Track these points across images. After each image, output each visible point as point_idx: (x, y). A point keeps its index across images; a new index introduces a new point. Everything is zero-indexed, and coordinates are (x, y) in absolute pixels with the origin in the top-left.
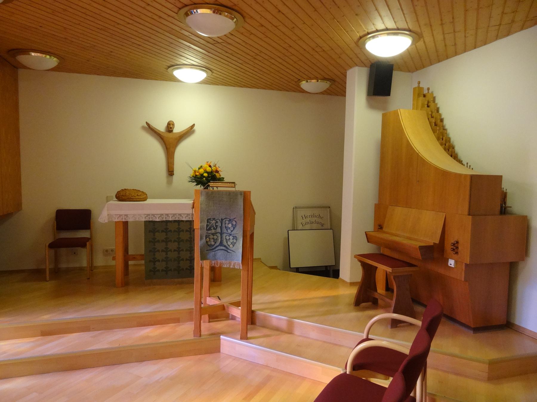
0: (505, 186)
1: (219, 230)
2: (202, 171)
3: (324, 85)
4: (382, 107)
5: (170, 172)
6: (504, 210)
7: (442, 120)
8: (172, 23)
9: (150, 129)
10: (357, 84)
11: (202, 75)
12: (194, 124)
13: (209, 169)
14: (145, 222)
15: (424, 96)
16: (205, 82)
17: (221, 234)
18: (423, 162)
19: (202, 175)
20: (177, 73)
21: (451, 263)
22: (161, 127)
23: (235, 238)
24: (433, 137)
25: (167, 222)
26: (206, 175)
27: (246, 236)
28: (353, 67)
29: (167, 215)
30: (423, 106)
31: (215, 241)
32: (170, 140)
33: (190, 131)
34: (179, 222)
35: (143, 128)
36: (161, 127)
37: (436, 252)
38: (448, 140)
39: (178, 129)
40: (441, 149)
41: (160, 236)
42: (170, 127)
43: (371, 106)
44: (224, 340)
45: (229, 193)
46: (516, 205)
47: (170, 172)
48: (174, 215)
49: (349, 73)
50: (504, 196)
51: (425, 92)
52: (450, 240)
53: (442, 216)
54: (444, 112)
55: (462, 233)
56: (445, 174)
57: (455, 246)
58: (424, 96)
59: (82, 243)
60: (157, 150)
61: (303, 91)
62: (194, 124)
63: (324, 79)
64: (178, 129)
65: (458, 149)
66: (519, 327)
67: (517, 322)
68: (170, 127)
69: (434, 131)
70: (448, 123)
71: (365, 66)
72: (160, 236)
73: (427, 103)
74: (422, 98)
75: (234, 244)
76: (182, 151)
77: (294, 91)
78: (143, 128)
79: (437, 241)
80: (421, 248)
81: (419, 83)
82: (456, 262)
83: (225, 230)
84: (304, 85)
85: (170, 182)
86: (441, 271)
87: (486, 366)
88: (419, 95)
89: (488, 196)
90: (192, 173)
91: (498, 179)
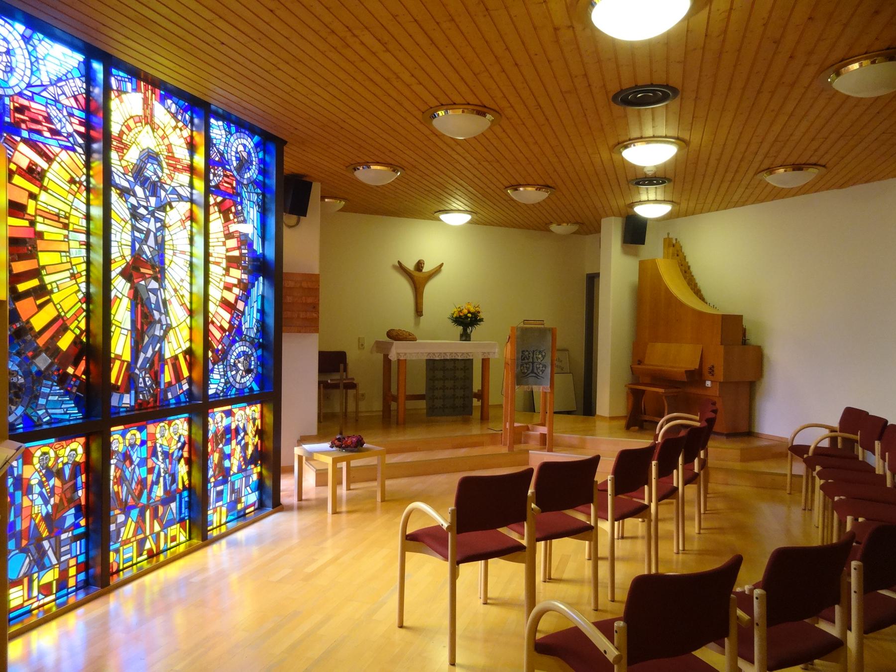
0: (745, 323)
1: (531, 360)
2: (465, 311)
3: (574, 228)
4: (635, 254)
5: (419, 312)
6: (744, 342)
7: (689, 267)
9: (401, 268)
11: (467, 218)
12: (442, 264)
14: (427, 360)
15: (674, 246)
16: (470, 222)
17: (533, 363)
18: (681, 304)
19: (466, 315)
20: (443, 217)
21: (708, 383)
22: (410, 266)
23: (545, 366)
24: (685, 283)
26: (469, 315)
30: (673, 255)
31: (528, 369)
32: (417, 277)
33: (438, 270)
34: (455, 360)
35: (394, 267)
36: (410, 266)
37: (696, 377)
38: (696, 285)
40: (692, 292)
41: (439, 374)
42: (419, 266)
43: (626, 252)
45: (540, 329)
46: (753, 339)
47: (419, 312)
48: (463, 354)
50: (744, 331)
51: (674, 242)
52: (707, 366)
53: (700, 347)
54: (690, 260)
55: (717, 358)
56: (701, 314)
57: (712, 370)
58: (674, 246)
59: (485, 362)
60: (404, 287)
61: (550, 231)
62: (442, 264)
63: (577, 223)
65: (703, 292)
68: (419, 266)
69: (685, 278)
70: (695, 270)
72: (439, 374)
73: (675, 250)
75: (543, 371)
76: (431, 289)
78: (394, 267)
79: (697, 367)
80: (686, 372)
81: (668, 234)
82: (712, 382)
83: (535, 360)
84: (554, 228)
85: (417, 323)
86: (700, 392)
87: (739, 452)
88: (669, 246)
89: (733, 331)
91: (739, 318)
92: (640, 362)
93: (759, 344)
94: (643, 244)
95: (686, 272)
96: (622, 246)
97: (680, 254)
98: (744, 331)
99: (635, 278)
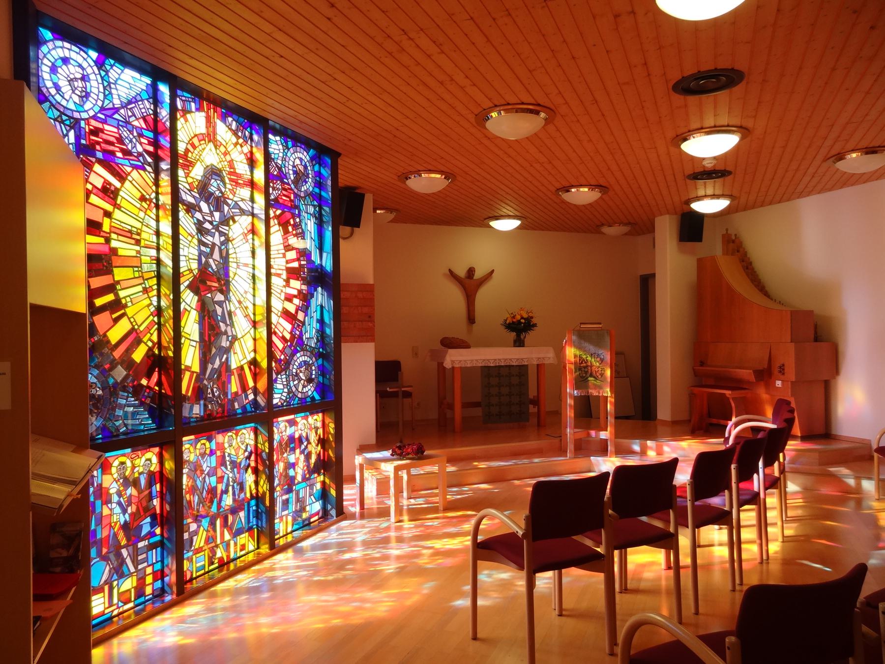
2: (519, 317)
7: (751, 263)
8: (61, 12)
10: (666, 229)
12: (493, 271)
13: (525, 316)
19: (519, 322)
21: (779, 383)
22: (462, 272)
25: (500, 367)
26: (523, 321)
27: (104, 628)
28: (532, 136)
29: (500, 360)
32: (470, 284)
34: (510, 367)
36: (462, 272)
39: (478, 274)
42: (471, 272)
44: (520, 527)
48: (506, 360)
49: (656, 219)
51: (733, 238)
58: (733, 242)
60: (455, 296)
64: (478, 274)
66: (836, 435)
67: (834, 432)
68: (471, 272)
71: (676, 214)
74: (731, 244)
76: (483, 296)
77: (592, 233)
78: (445, 275)
81: (727, 230)
84: (606, 230)
90: (501, 321)
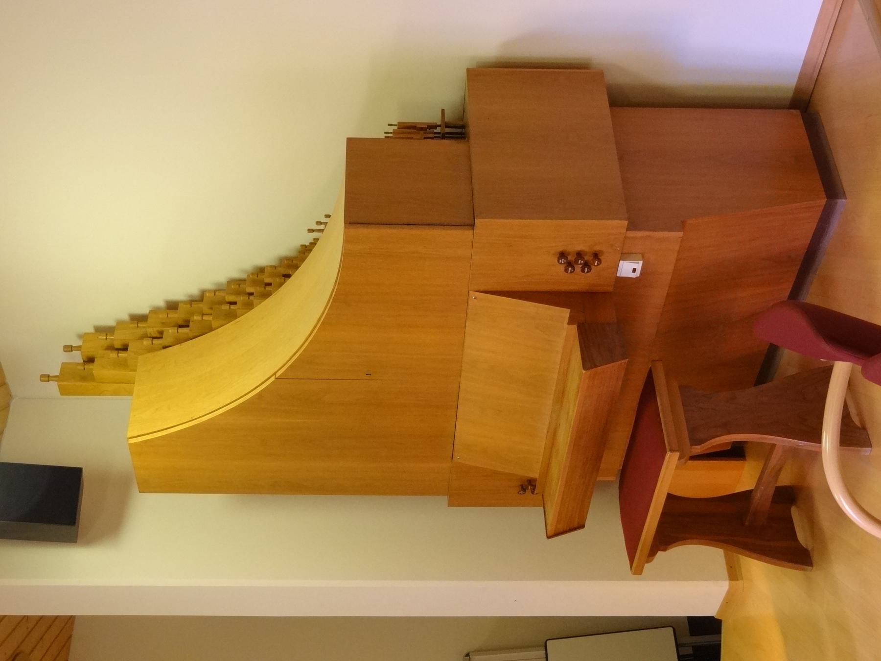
0: (376, 129)
6: (454, 130)
15: (90, 360)
18: (304, 363)
30: (124, 365)
38: (236, 285)
40: (263, 308)
43: (112, 528)
46: (436, 99)
51: (77, 357)
53: (479, 301)
57: (570, 260)
65: (266, 255)
79: (565, 313)
80: (588, 362)
81: (46, 378)
82: (625, 255)
86: (657, 296)
91: (358, 150)
92: (528, 487)
93: (463, 74)
94: (353, 144)
95: (187, 321)
96: (90, 541)
97: (118, 339)
98: (408, 130)
99: (210, 505)
